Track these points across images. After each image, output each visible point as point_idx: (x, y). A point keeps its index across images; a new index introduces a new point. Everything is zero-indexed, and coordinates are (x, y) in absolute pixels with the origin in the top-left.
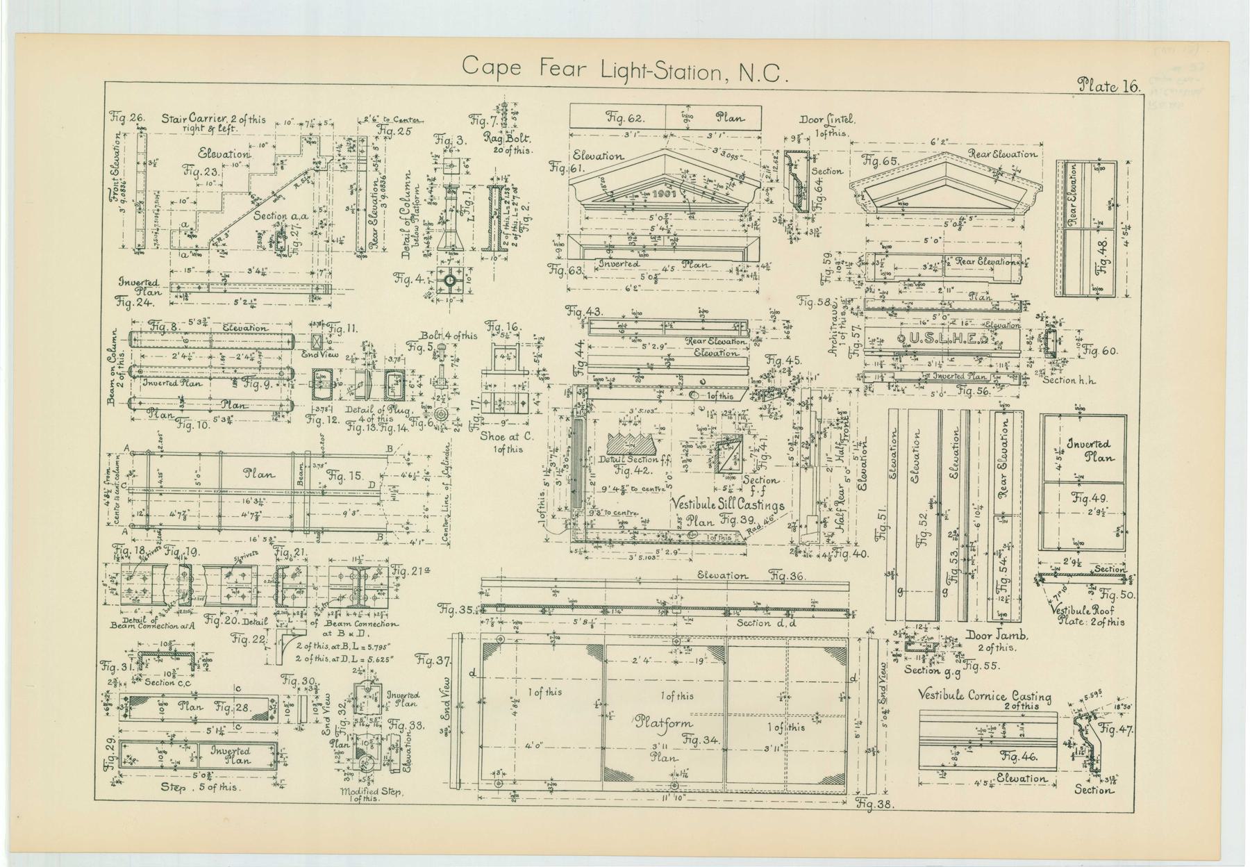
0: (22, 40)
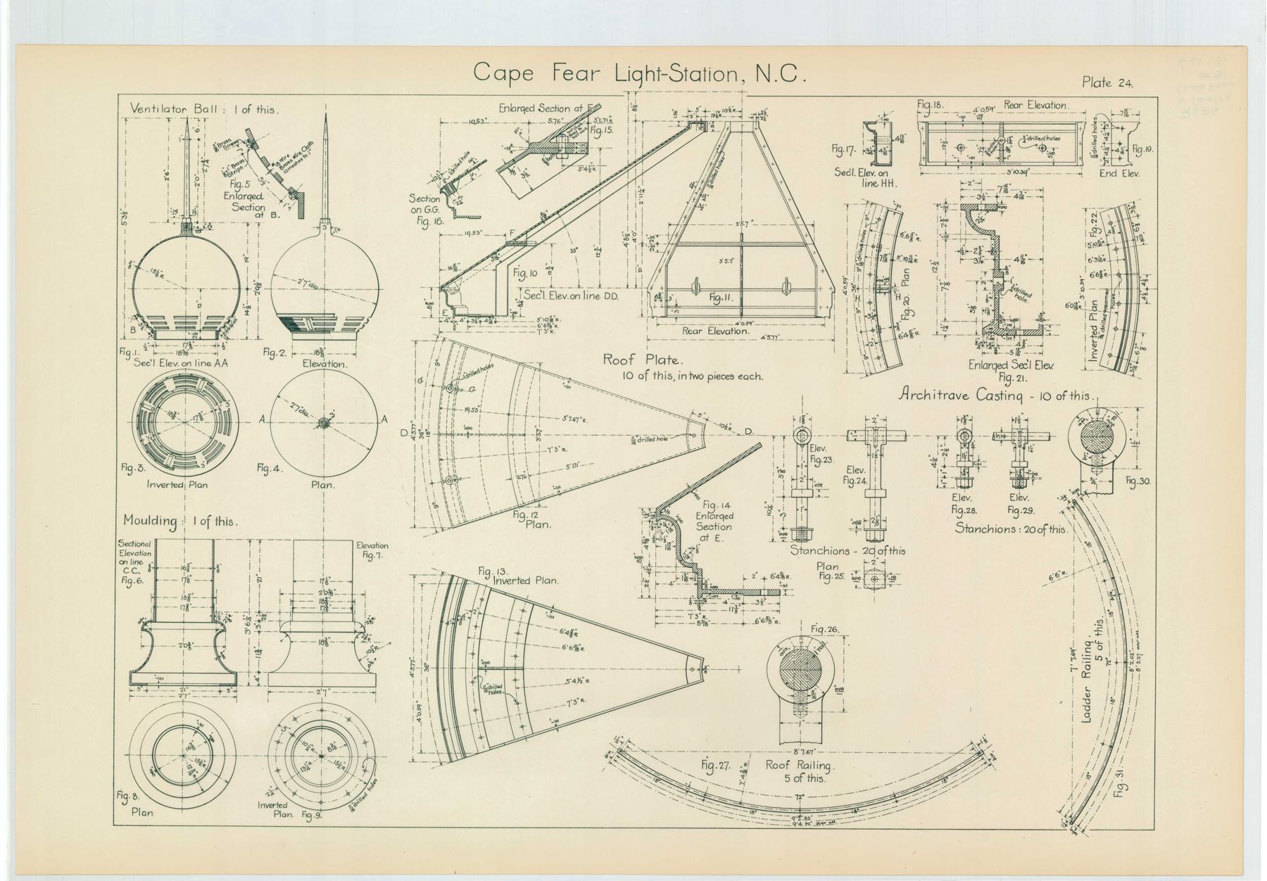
0: (23, 52)
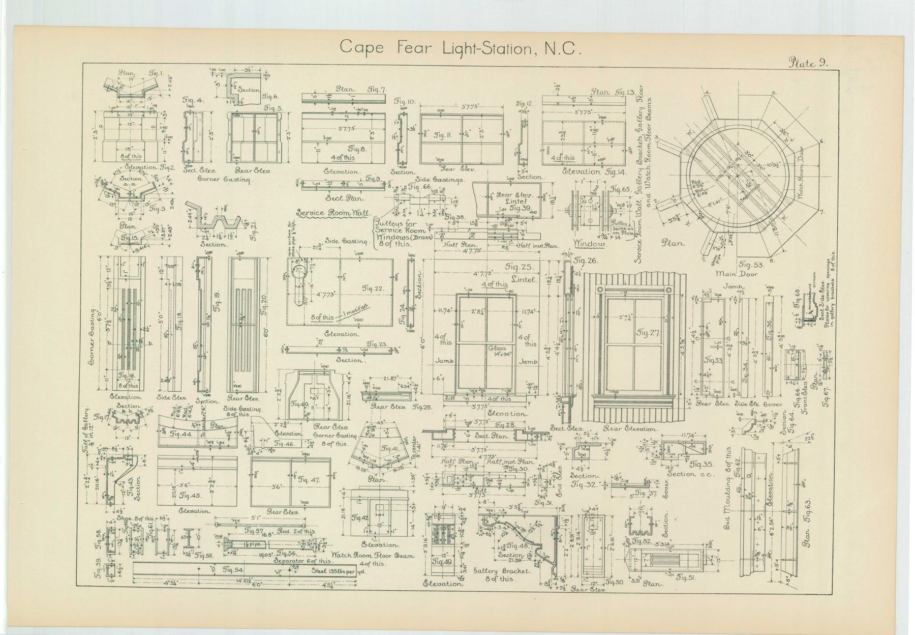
0: (17, 31)
